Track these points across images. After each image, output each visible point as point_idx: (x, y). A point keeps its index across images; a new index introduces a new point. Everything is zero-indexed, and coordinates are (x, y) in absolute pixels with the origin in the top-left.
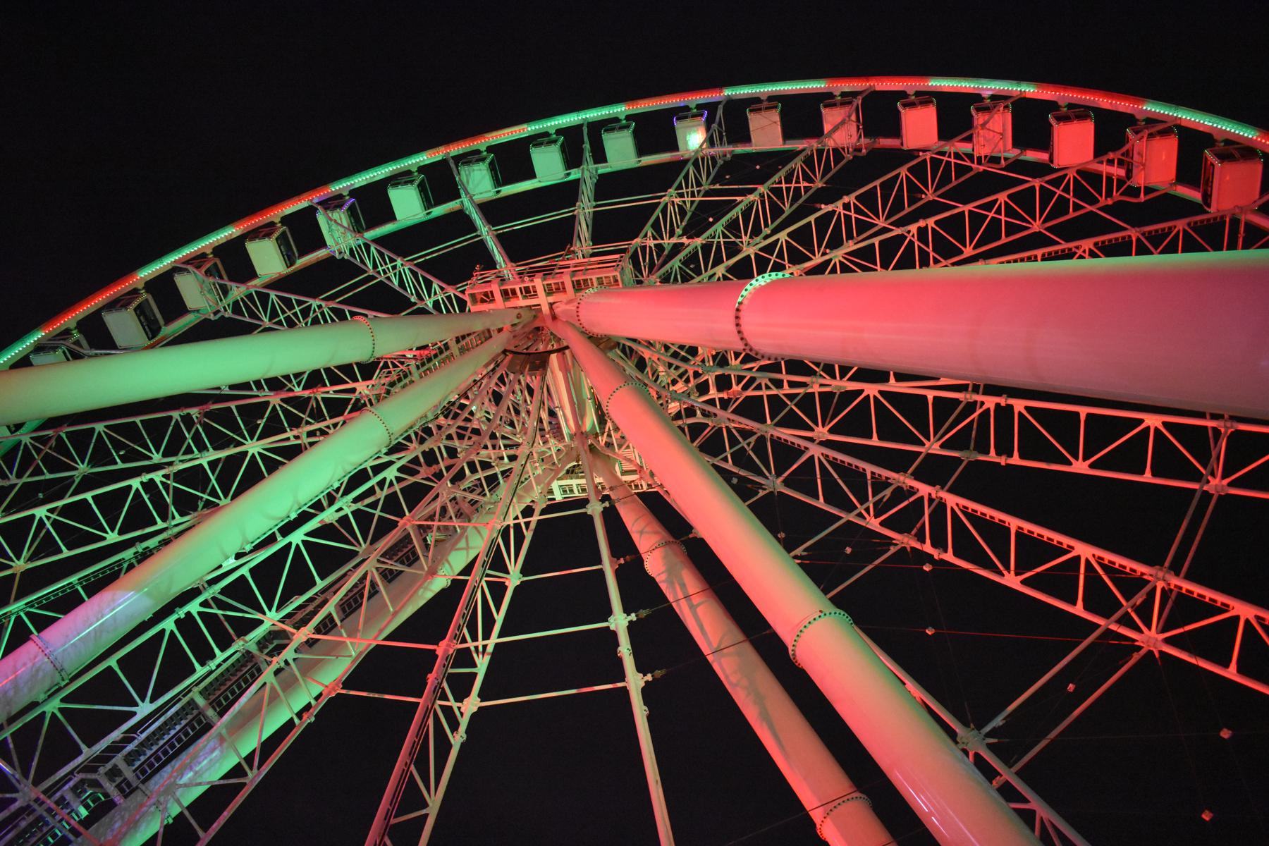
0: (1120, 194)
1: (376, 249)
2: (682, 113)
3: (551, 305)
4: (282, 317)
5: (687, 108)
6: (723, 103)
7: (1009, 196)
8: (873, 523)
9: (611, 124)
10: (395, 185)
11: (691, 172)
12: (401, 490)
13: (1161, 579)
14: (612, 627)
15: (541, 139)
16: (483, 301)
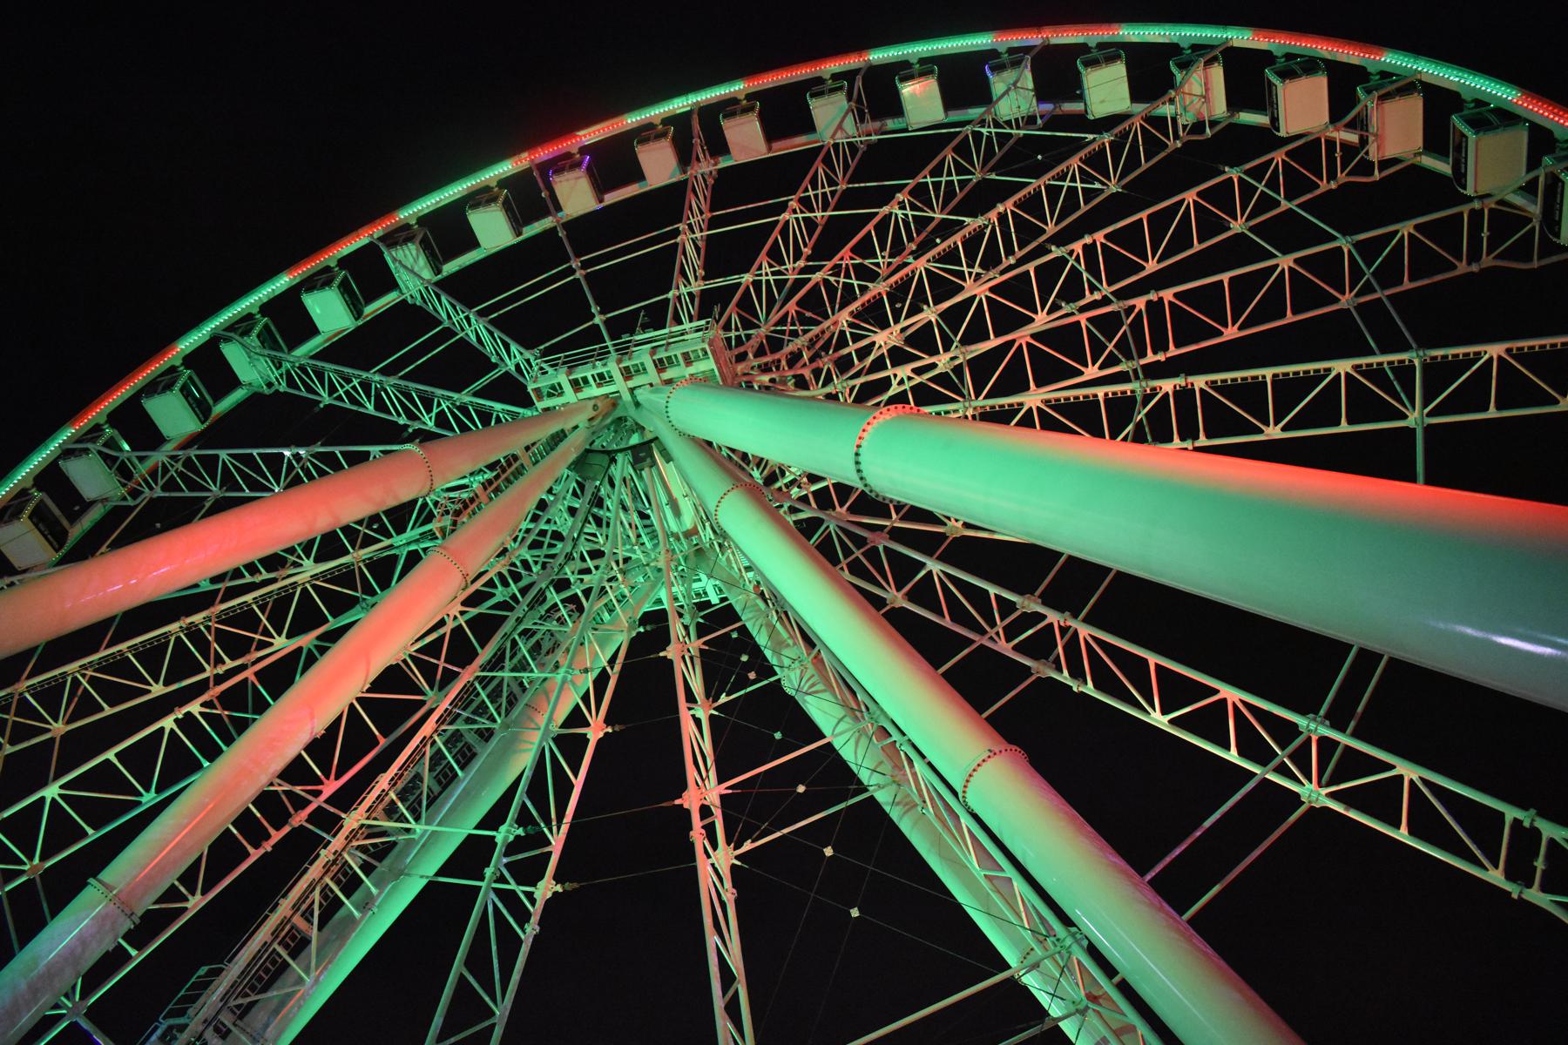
0: (1347, 175)
1: (367, 408)
2: (816, 86)
3: (632, 390)
4: (341, 392)
5: (819, 80)
6: (862, 72)
7: (1199, 194)
8: (1005, 647)
9: (729, 107)
10: (476, 206)
11: (820, 171)
12: (466, 622)
13: (1313, 727)
14: (686, 806)
15: (646, 133)
16: (550, 395)
